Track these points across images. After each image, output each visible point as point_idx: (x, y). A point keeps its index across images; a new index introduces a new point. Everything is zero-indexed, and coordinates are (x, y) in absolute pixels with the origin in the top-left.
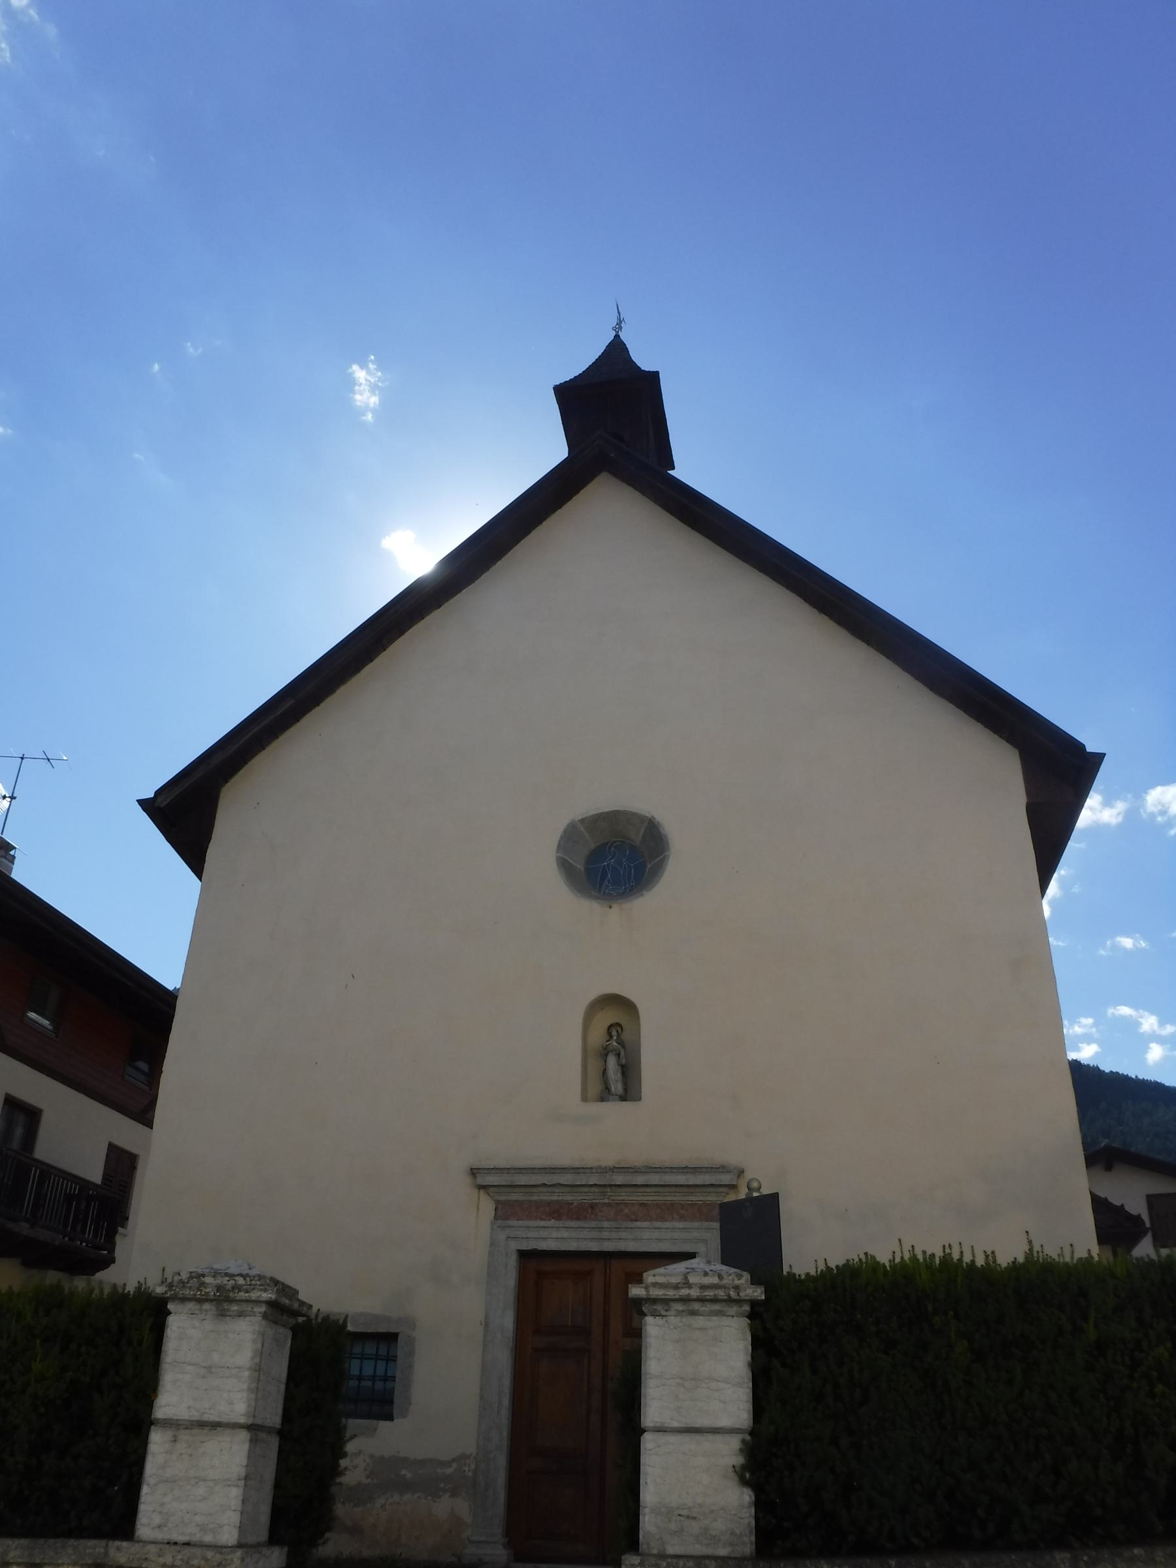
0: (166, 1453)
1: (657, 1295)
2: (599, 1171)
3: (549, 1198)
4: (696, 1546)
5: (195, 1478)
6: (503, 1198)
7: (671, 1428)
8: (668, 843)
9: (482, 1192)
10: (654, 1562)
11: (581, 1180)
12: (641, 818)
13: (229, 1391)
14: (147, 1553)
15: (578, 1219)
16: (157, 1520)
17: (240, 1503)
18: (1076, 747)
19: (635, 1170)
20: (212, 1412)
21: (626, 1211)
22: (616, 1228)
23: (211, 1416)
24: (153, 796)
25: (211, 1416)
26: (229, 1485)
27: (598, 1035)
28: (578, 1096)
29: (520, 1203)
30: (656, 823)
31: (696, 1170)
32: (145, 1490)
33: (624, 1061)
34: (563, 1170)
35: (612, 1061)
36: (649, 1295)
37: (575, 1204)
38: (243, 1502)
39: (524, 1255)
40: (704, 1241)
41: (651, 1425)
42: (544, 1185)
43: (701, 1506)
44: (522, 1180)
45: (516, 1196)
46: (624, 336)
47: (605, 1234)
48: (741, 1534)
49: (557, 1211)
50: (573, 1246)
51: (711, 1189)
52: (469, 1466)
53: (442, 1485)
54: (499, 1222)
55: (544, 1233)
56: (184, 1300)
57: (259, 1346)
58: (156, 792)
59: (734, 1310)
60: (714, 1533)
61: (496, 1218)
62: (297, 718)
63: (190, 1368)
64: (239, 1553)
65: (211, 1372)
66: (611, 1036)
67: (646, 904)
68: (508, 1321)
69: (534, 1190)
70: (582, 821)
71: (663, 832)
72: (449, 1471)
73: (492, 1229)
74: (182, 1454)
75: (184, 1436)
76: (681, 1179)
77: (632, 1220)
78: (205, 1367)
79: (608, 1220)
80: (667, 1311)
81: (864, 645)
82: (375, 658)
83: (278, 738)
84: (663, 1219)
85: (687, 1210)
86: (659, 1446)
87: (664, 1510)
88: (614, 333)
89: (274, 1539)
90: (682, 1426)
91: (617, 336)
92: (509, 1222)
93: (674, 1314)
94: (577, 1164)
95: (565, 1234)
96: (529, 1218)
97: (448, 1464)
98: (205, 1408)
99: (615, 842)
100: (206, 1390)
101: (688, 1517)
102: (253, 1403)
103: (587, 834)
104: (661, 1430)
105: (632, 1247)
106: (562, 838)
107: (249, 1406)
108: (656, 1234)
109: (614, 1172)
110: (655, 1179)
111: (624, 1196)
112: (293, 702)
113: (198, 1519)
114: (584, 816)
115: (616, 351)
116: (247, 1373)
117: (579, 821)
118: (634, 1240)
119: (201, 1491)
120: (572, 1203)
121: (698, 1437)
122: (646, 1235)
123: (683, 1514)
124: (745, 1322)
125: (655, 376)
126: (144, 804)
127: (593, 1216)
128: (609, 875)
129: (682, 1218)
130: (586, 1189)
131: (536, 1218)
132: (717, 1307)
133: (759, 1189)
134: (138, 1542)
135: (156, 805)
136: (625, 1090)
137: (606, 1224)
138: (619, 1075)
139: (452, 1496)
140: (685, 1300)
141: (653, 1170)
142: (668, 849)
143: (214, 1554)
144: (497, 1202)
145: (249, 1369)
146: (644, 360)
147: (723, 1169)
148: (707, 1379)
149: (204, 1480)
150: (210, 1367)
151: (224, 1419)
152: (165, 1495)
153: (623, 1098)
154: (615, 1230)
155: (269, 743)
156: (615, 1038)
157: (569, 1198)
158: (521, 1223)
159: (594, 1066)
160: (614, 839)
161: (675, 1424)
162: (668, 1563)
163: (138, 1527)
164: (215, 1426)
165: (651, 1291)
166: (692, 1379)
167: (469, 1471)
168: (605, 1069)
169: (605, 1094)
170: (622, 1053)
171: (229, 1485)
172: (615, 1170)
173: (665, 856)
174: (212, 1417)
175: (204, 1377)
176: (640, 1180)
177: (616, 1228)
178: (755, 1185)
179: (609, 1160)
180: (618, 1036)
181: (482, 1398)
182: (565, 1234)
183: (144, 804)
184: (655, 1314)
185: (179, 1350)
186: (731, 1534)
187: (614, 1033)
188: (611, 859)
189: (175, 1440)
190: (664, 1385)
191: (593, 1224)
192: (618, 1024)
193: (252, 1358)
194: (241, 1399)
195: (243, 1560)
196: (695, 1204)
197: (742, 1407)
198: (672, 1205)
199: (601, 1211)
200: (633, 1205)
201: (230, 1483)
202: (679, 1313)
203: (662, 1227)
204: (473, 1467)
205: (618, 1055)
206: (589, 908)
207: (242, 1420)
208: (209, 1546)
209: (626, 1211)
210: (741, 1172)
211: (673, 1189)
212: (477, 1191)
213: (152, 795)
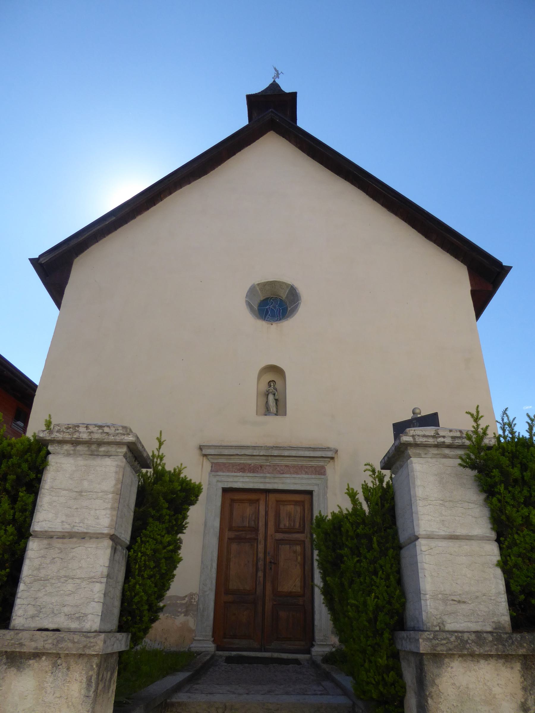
1: (422, 442)
2: (266, 448)
3: (238, 462)
5: (65, 577)
6: (216, 461)
8: (300, 297)
9: (205, 458)
10: (445, 637)
11: (256, 453)
12: (287, 285)
13: (96, 510)
14: (21, 639)
15: (254, 472)
16: (31, 611)
17: (102, 596)
18: (497, 263)
19: (284, 448)
21: (278, 469)
22: (273, 477)
23: (80, 528)
24: (38, 257)
25: (80, 528)
26: (94, 582)
27: (264, 387)
28: (256, 414)
29: (224, 464)
30: (295, 288)
31: (314, 449)
32: (22, 587)
33: (277, 397)
34: (247, 447)
35: (271, 397)
36: (416, 441)
37: (252, 465)
38: (105, 595)
39: (225, 491)
40: (317, 485)
41: (424, 533)
42: (237, 455)
44: (226, 452)
45: (222, 460)
47: (267, 480)
49: (243, 469)
50: (251, 486)
51: (321, 459)
52: (194, 599)
53: (180, 610)
54: (213, 473)
55: (236, 479)
56: (61, 442)
57: (121, 477)
58: (39, 256)
61: (211, 471)
62: (116, 229)
64: (103, 636)
65: (82, 496)
66: (270, 386)
67: (287, 324)
68: (217, 523)
69: (232, 457)
70: (258, 284)
71: (298, 292)
72: (184, 602)
73: (209, 477)
75: (57, 544)
76: (307, 454)
77: (281, 474)
78: (76, 492)
79: (269, 473)
80: (426, 454)
82: (157, 203)
83: (105, 237)
84: (297, 473)
85: (309, 469)
86: (431, 549)
88: (273, 80)
89: (121, 629)
90: (447, 534)
92: (218, 473)
93: (430, 457)
94: (254, 445)
95: (247, 480)
96: (229, 471)
97: (183, 598)
98: (76, 522)
99: (273, 297)
100: (77, 508)
102: (115, 518)
103: (260, 292)
104: (430, 537)
105: (281, 487)
106: (248, 292)
107: (112, 520)
108: (293, 481)
109: (273, 449)
110: (294, 453)
111: (277, 461)
112: (114, 218)
113: (66, 610)
114: (260, 282)
116: (110, 496)
117: (257, 284)
118: (283, 483)
119: (70, 587)
120: (251, 465)
121: (458, 543)
122: (288, 481)
123: (455, 599)
126: (33, 261)
128: (269, 312)
129: (307, 473)
130: (258, 458)
131: (232, 472)
133: (420, 414)
134: (13, 630)
135: (39, 262)
136: (277, 412)
137: (268, 475)
138: (275, 404)
139: (185, 615)
141: (293, 449)
142: (300, 299)
143: (516, 468)
144: (212, 463)
145: (113, 493)
147: (328, 449)
148: (460, 501)
149: (73, 578)
150: (81, 492)
152: (39, 590)
153: (276, 415)
154: (272, 478)
155: (101, 239)
156: (272, 387)
157: (249, 462)
158: (224, 474)
159: (263, 400)
160: (272, 296)
161: (442, 533)
162: (456, 637)
163: (14, 618)
164: (83, 536)
165: (417, 439)
167: (194, 602)
168: (267, 402)
169: (267, 411)
170: (276, 394)
172: (274, 448)
173: (298, 304)
174: (82, 529)
175: (75, 499)
176: (286, 453)
177: (273, 477)
178: (417, 411)
179: (270, 442)
180: (274, 385)
181: (202, 562)
182: (247, 480)
183: (33, 261)
184: (419, 456)
185: (56, 479)
187: (272, 384)
188: (271, 305)
191: (262, 475)
192: (273, 381)
193: (116, 485)
195: (105, 642)
196: (313, 466)
198: (302, 466)
199: (266, 469)
200: (282, 466)
202: (435, 456)
203: (297, 477)
204: (197, 600)
205: (274, 394)
206: (261, 324)
207: (106, 531)
208: (74, 632)
209: (278, 469)
210: (336, 451)
211: (302, 459)
212: (202, 457)
213: (37, 257)
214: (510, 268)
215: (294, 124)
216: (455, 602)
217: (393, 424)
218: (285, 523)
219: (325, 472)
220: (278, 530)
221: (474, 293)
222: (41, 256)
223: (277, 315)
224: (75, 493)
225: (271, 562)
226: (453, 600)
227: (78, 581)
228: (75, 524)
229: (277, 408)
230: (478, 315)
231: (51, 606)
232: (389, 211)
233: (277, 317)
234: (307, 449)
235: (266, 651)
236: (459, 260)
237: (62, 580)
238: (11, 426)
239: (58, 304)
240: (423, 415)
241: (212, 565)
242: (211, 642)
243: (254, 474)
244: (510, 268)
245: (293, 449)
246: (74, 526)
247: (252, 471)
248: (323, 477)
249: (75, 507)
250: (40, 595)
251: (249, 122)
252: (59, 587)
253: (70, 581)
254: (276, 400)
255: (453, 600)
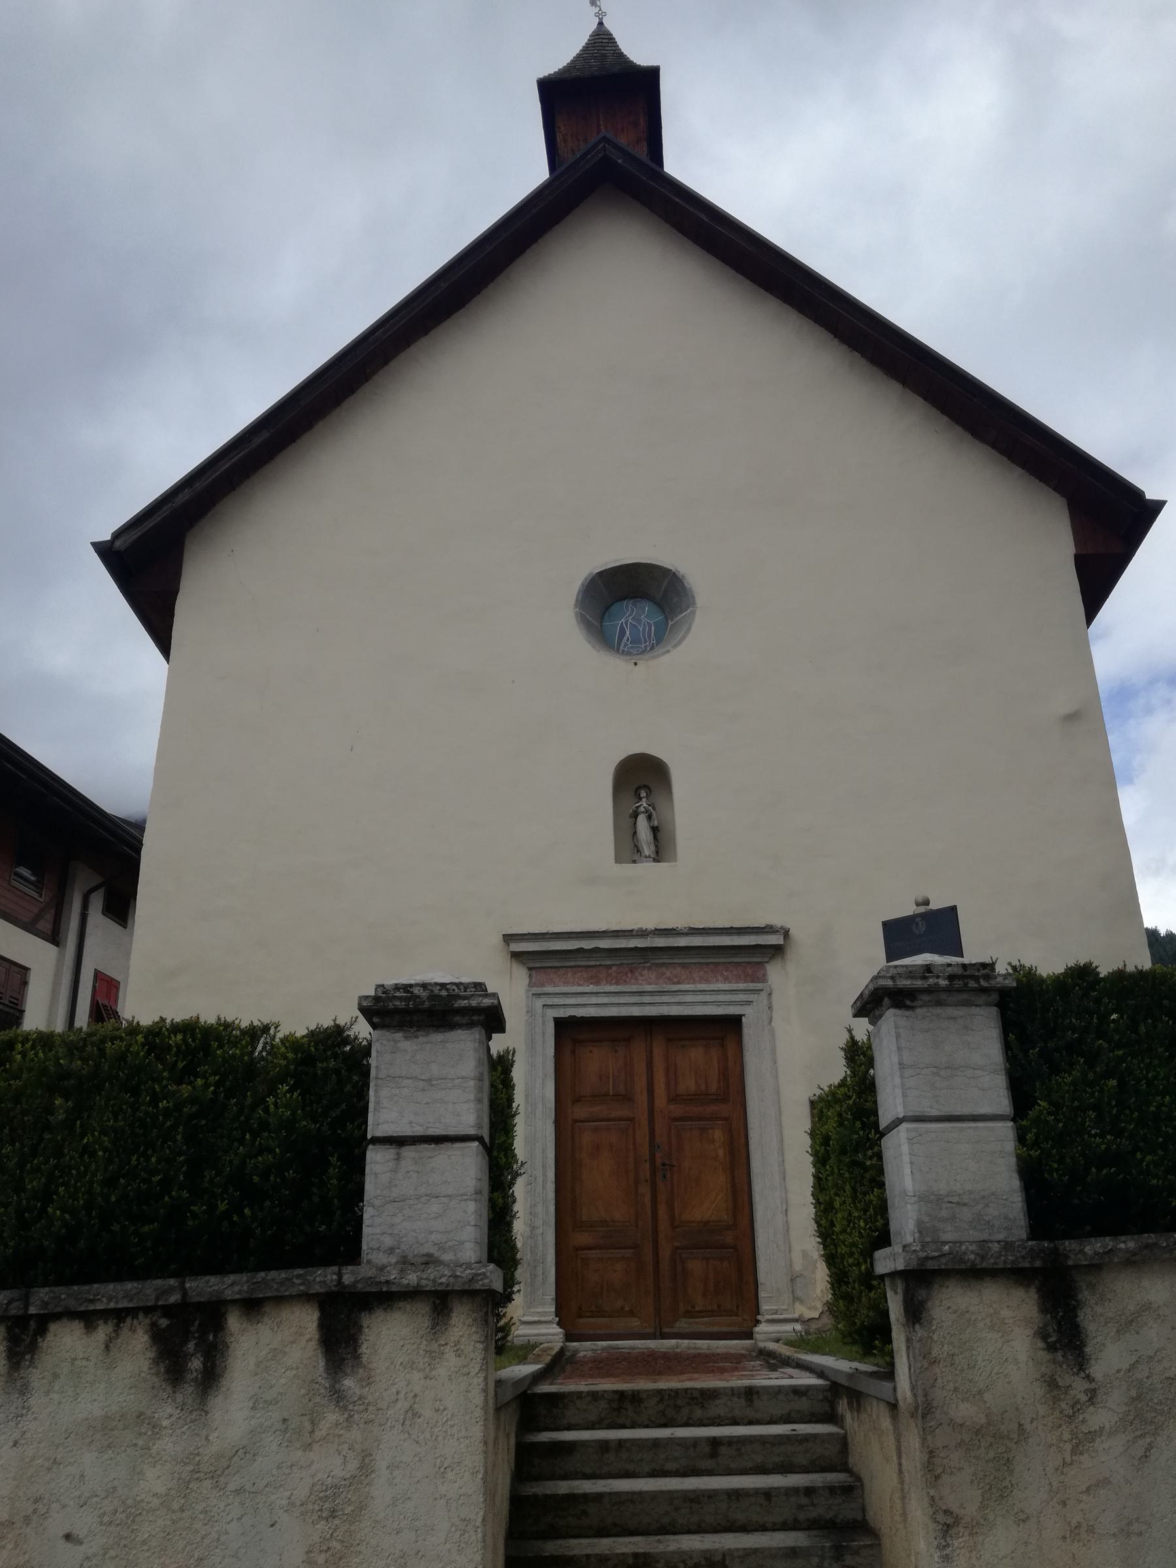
0: (391, 1171)
2: (640, 933)
4: (971, 1232)
7: (931, 1116)
13: (454, 1103)
18: (1132, 494)
20: (437, 1125)
25: (436, 1130)
26: (466, 1200)
33: (656, 823)
43: (971, 1192)
46: (609, 25)
48: (1015, 1218)
59: (983, 998)
60: (987, 1218)
63: (406, 1082)
65: (433, 1085)
74: (408, 1172)
75: (408, 1152)
81: (898, 386)
87: (932, 1197)
88: (597, 20)
91: (601, 24)
101: (958, 1203)
113: (433, 1237)
115: (602, 41)
116: (472, 1083)
119: (435, 1207)
123: (953, 1201)
124: (994, 1011)
125: (653, 75)
127: (633, 981)
128: (628, 632)
131: (573, 984)
132: (964, 996)
136: (657, 853)
140: (929, 991)
146: (639, 54)
147: (768, 930)
149: (437, 1197)
151: (451, 1132)
153: (656, 860)
161: (935, 1113)
166: (947, 1068)
170: (654, 814)
171: (466, 1200)
175: (423, 1090)
176: (682, 942)
186: (1005, 1218)
189: (398, 1158)
190: (918, 1074)
194: (468, 1110)
197: (1002, 1094)
201: (465, 1197)
214: (1157, 506)
215: (653, 165)
216: (953, 1205)
217: (885, 924)
218: (688, 1084)
219: (764, 975)
220: (674, 1098)
221: (1083, 564)
222: (117, 535)
223: (644, 638)
224: (422, 1082)
225: (664, 1164)
226: (949, 1202)
227: (444, 1200)
228: (429, 1125)
229: (656, 846)
230: (1091, 611)
231: (414, 1234)
232: (887, 374)
233: (646, 642)
234: (725, 931)
235: (663, 1336)
236: (1047, 484)
237: (423, 1199)
238: (9, 881)
239: (163, 641)
240: (934, 908)
241: (545, 1175)
242: (555, 1325)
243: (619, 987)
244: (1157, 506)
245: (695, 931)
246: (428, 1128)
247: (613, 982)
248: (759, 986)
249: (424, 1102)
250: (397, 1220)
251: (550, 175)
252: (420, 1210)
253: (433, 1200)
254: (655, 830)
255: (949, 1202)
